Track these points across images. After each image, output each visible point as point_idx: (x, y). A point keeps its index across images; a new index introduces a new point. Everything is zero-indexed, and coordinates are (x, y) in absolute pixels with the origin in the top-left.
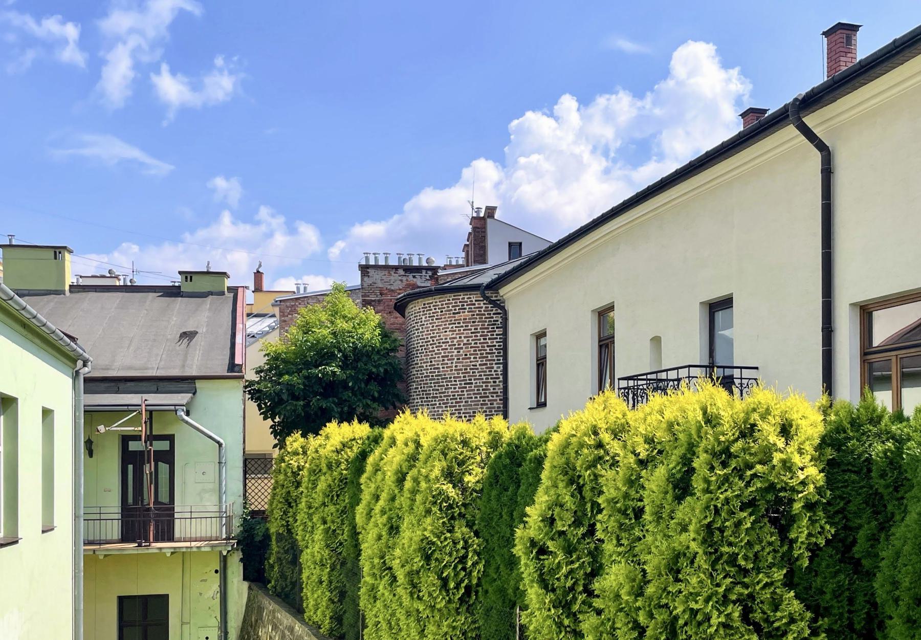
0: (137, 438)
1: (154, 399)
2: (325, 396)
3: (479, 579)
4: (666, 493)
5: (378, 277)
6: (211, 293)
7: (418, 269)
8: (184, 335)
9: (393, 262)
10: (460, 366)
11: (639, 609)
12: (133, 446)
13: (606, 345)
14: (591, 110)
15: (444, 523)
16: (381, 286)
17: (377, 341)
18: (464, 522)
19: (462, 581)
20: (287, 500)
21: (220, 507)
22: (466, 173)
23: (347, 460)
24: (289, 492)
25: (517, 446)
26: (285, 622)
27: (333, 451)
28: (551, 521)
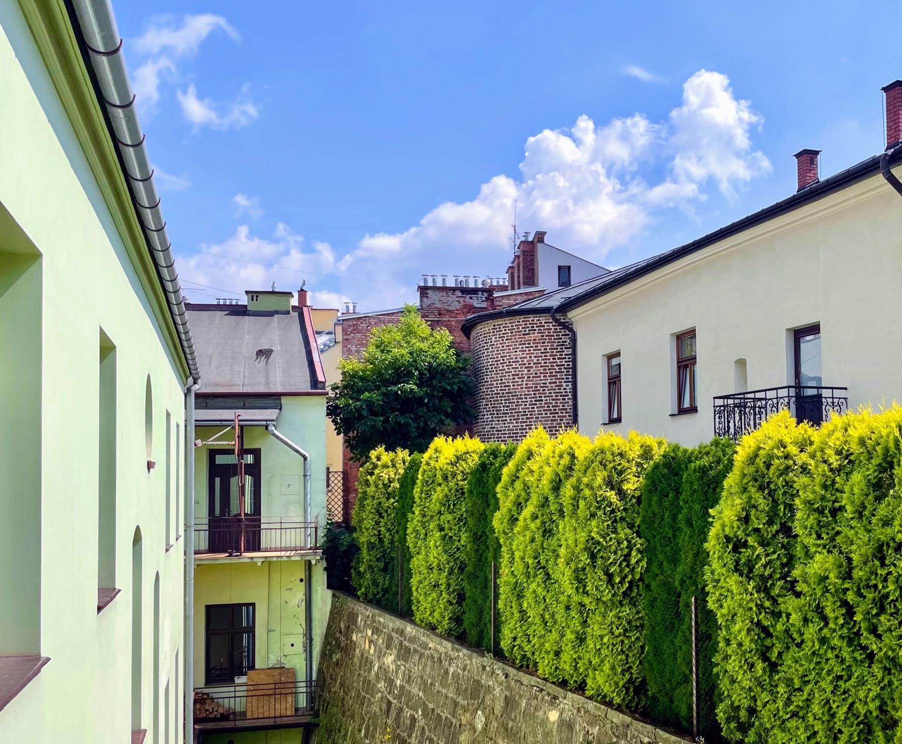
0: (229, 452)
1: (247, 414)
2: (402, 412)
3: (641, 574)
4: (867, 495)
5: (436, 298)
6: (277, 312)
7: (475, 291)
8: (260, 353)
9: (450, 283)
10: (530, 384)
11: (848, 589)
12: (220, 460)
13: (685, 365)
14: (607, 131)
15: (608, 525)
16: (439, 306)
17: (452, 361)
18: (625, 525)
19: (626, 576)
20: (378, 511)
21: (305, 517)
22: (486, 189)
23: (462, 472)
24: (380, 503)
25: (673, 458)
26: (391, 625)
27: (448, 464)
28: (746, 520)
